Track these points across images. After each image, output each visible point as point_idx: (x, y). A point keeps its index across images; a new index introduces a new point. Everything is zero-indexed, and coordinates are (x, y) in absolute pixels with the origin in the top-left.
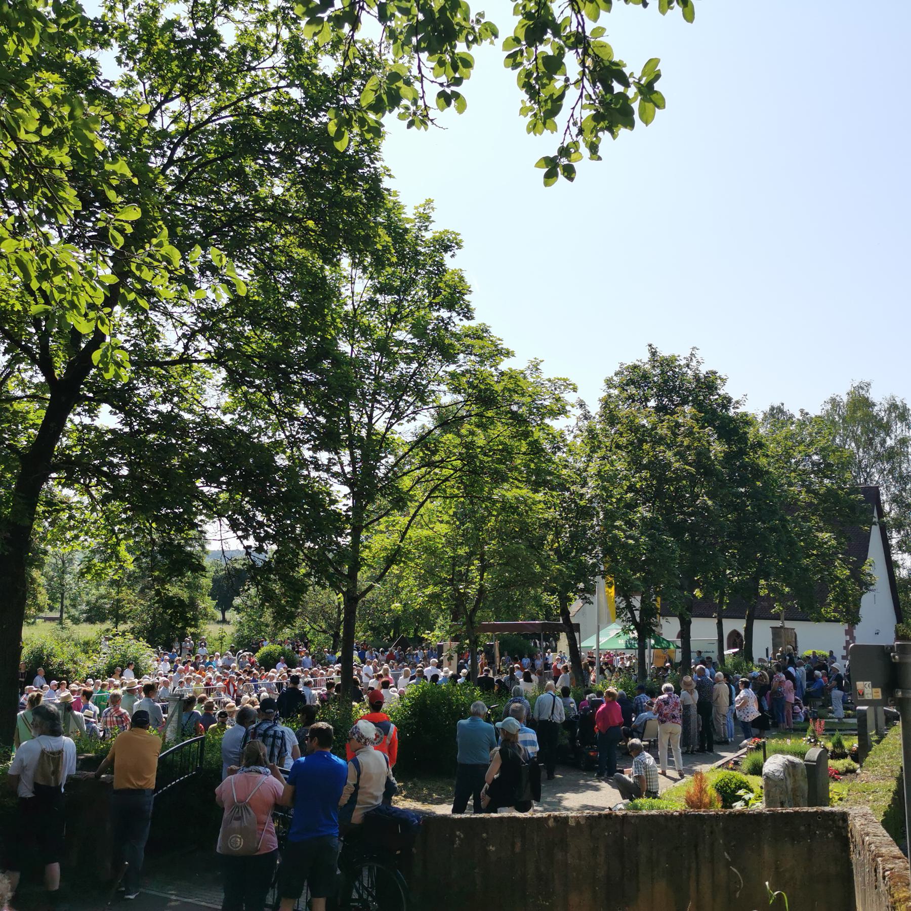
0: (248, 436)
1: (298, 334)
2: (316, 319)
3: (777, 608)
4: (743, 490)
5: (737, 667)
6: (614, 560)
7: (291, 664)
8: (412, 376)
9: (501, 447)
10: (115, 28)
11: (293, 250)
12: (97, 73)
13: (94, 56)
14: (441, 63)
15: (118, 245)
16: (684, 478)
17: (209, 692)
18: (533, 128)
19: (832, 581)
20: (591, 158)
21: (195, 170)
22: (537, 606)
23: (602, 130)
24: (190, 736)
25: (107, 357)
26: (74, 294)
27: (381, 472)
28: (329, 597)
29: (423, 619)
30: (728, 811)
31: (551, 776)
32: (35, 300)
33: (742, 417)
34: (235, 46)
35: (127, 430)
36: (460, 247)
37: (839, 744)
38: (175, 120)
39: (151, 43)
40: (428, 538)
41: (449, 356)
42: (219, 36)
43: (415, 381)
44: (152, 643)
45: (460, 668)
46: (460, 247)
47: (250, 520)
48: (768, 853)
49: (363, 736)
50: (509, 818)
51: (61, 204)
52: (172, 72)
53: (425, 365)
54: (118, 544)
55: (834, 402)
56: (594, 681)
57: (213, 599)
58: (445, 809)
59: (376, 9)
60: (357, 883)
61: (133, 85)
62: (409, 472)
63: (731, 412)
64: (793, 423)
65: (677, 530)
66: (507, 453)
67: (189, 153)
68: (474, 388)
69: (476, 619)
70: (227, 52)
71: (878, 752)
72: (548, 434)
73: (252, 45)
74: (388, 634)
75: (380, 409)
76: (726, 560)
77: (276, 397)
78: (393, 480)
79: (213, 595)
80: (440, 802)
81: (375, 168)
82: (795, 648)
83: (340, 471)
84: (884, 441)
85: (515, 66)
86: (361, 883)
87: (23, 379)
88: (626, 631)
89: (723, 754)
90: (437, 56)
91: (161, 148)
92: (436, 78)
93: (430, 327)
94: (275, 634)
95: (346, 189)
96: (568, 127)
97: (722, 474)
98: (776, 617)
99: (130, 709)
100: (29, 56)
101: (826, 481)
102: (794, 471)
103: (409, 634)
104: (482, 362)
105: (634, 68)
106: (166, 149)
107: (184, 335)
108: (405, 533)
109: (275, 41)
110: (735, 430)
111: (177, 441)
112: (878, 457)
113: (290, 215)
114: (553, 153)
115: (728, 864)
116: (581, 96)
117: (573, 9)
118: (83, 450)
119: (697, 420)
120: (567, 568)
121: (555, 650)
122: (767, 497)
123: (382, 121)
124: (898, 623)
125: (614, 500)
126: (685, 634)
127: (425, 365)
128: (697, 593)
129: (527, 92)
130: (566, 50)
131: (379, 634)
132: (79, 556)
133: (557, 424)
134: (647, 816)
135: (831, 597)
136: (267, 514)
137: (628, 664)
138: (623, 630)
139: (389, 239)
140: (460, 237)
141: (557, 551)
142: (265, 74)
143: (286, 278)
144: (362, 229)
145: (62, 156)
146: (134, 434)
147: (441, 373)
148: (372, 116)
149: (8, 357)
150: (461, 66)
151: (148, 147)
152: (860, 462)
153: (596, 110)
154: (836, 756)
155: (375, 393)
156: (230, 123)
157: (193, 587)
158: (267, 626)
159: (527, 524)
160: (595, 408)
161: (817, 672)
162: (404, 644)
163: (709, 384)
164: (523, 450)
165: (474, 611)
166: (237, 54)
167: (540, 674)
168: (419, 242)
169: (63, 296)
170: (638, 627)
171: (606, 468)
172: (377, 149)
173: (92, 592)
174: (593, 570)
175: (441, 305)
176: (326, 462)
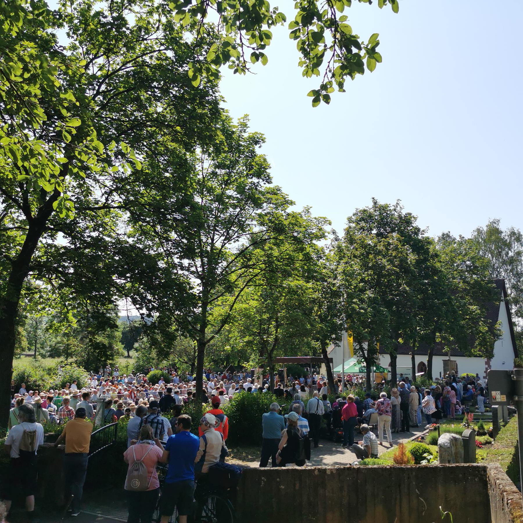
0: (142, 250)
1: (171, 192)
2: (182, 183)
3: (446, 349)
4: (427, 281)
5: (423, 383)
6: (353, 321)
7: (167, 381)
8: (236, 216)
9: (287, 257)
10: (66, 16)
11: (168, 144)
12: (56, 42)
13: (54, 32)
14: (253, 36)
15: (68, 140)
16: (393, 274)
17: (120, 397)
18: (306, 73)
19: (478, 334)
20: (339, 91)
21: (112, 97)
22: (308, 348)
23: (346, 74)
24: (109, 423)
25: (61, 205)
26: (42, 169)
27: (219, 271)
28: (189, 343)
29: (243, 355)
30: (418, 466)
31: (316, 446)
32: (20, 172)
33: (426, 239)
34: (135, 27)
35: (73, 247)
36: (264, 142)
37: (481, 427)
38: (101, 69)
39: (87, 25)
40: (246, 309)
41: (258, 204)
42: (126, 20)
43: (238, 219)
44: (87, 369)
45: (264, 383)
46: (264, 142)
47: (143, 298)
48: (441, 490)
49: (208, 423)
50: (292, 469)
51: (35, 117)
52: (99, 42)
53: (244, 209)
54: (68, 312)
55: (479, 231)
56: (341, 391)
57: (122, 344)
58: (255, 465)
59: (216, 5)
60: (205, 507)
61: (76, 49)
62: (235, 271)
63: (420, 237)
64: (455, 243)
65: (389, 304)
66: (291, 260)
67: (108, 88)
68: (272, 222)
69: (273, 355)
70: (130, 30)
71: (504, 432)
72: (315, 249)
73: (145, 26)
74: (223, 364)
75: (218, 235)
76: (417, 322)
77: (158, 228)
78: (226, 276)
79: (122, 342)
80: (252, 460)
81: (215, 97)
82: (457, 372)
83: (195, 270)
84: (507, 253)
85: (296, 38)
86: (207, 507)
87: (13, 218)
88: (359, 362)
89: (415, 433)
90: (251, 32)
91: (93, 85)
92: (250, 45)
93: (247, 188)
94: (158, 364)
95: (199, 108)
96: (326, 73)
97: (415, 272)
98: (446, 354)
99: (75, 407)
100: (16, 32)
101: (474, 276)
102: (456, 270)
103: (235, 364)
104: (276, 208)
105: (364, 39)
106: (95, 85)
107: (106, 192)
108: (233, 306)
109: (158, 24)
110: (422, 247)
111: (102, 253)
112: (504, 263)
113: (166, 123)
114: (318, 88)
115: (418, 496)
116: (333, 55)
117: (329, 5)
118: (47, 259)
119: (400, 241)
120: (326, 326)
121: (318, 373)
122: (440, 286)
123: (220, 69)
124: (516, 357)
125: (353, 287)
126: (393, 364)
127: (244, 209)
128: (400, 340)
129: (302, 53)
130: (325, 28)
131: (217, 364)
132: (45, 319)
133: (320, 244)
134: (372, 468)
135: (477, 342)
136: (153, 295)
137: (360, 381)
138: (357, 361)
139: (223, 137)
140: (264, 136)
141: (320, 316)
142: (152, 42)
143: (164, 160)
144: (208, 131)
145: (35, 90)
146: (77, 249)
147: (253, 214)
148: (213, 67)
149: (4, 205)
150: (264, 38)
151: (85, 84)
152: (494, 265)
153: (342, 63)
154: (480, 434)
155: (215, 226)
156: (132, 70)
157: (111, 337)
158: (153, 359)
159: (303, 301)
160: (341, 235)
161: (469, 386)
162: (232, 370)
163: (407, 220)
164: (300, 258)
165: (272, 350)
166: (136, 31)
167: (310, 387)
168: (241, 139)
169: (36, 170)
170: (366, 360)
171: (348, 269)
172: (216, 86)
173: (53, 340)
174: (340, 327)
175: (253, 175)
176: (187, 265)
